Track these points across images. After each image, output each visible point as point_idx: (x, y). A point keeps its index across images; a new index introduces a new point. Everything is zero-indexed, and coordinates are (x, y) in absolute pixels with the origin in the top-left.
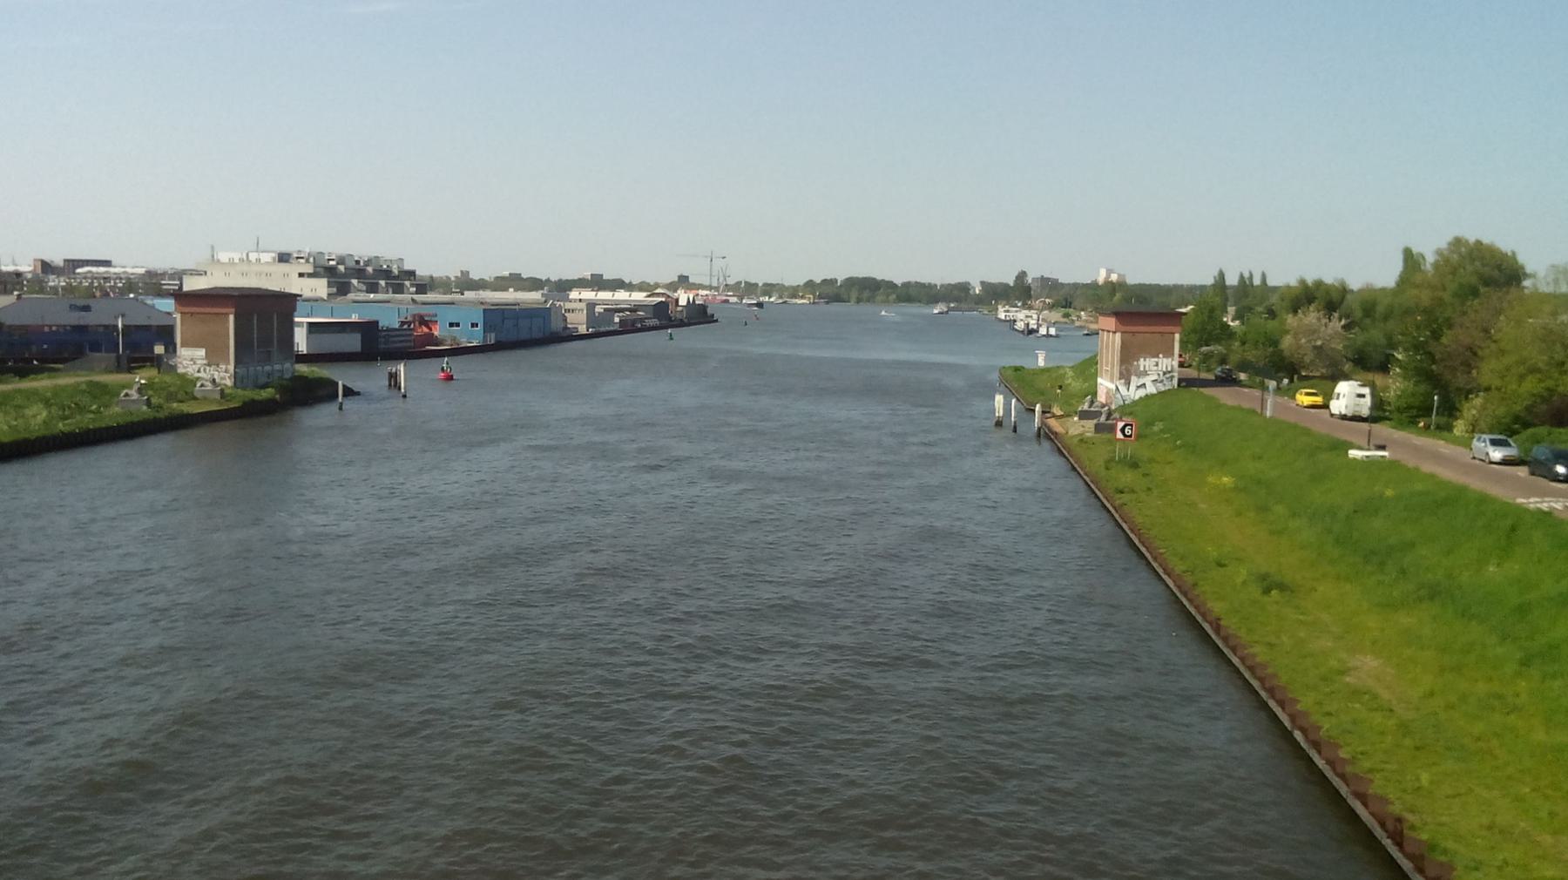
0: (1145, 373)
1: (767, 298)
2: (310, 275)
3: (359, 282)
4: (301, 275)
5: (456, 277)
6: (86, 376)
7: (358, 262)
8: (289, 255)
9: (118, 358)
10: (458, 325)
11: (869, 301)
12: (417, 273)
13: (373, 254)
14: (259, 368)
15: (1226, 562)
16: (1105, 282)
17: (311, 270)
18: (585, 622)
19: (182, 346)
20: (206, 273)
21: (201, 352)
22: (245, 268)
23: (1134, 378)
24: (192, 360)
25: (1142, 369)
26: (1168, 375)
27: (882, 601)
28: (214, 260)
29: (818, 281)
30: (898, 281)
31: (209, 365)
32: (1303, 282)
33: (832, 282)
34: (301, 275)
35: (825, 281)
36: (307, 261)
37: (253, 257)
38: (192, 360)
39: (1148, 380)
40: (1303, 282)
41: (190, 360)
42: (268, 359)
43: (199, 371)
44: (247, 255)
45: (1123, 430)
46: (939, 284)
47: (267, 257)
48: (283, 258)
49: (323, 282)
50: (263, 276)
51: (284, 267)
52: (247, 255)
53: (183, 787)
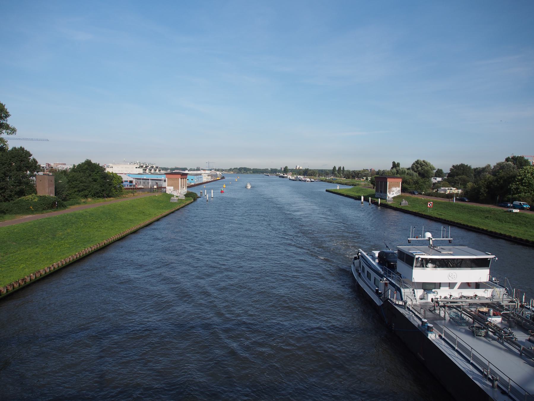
0: (394, 191)
1: (282, 175)
2: (139, 168)
4: (136, 168)
6: (445, 200)
16: (12, 150)
18: (232, 281)
20: (112, 167)
23: (391, 192)
24: (170, 189)
25: (393, 190)
26: (399, 192)
27: (275, 272)
29: (233, 168)
30: (252, 168)
31: (174, 191)
34: (136, 168)
35: (253, 169)
39: (394, 193)
43: (172, 192)
45: (429, 205)
53: (175, 374)
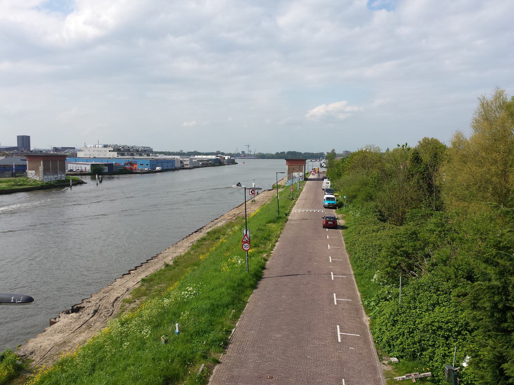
2: (112, 151)
3: (118, 154)
4: (110, 151)
5: (353, 152)
7: (129, 147)
8: (107, 145)
9: (12, 173)
10: (143, 165)
11: (416, 158)
12: (337, 152)
13: (133, 145)
14: (52, 176)
15: (221, 361)
17: (112, 150)
19: (29, 170)
21: (34, 172)
22: (94, 149)
24: (31, 174)
28: (86, 147)
30: (303, 152)
32: (419, 142)
33: (284, 153)
34: (110, 151)
36: (112, 147)
37: (97, 146)
38: (31, 174)
40: (419, 142)
41: (31, 174)
42: (56, 173)
44: (95, 145)
46: (265, 154)
47: (100, 146)
48: (105, 146)
49: (116, 153)
50: (99, 151)
51: (105, 149)
52: (95, 145)
